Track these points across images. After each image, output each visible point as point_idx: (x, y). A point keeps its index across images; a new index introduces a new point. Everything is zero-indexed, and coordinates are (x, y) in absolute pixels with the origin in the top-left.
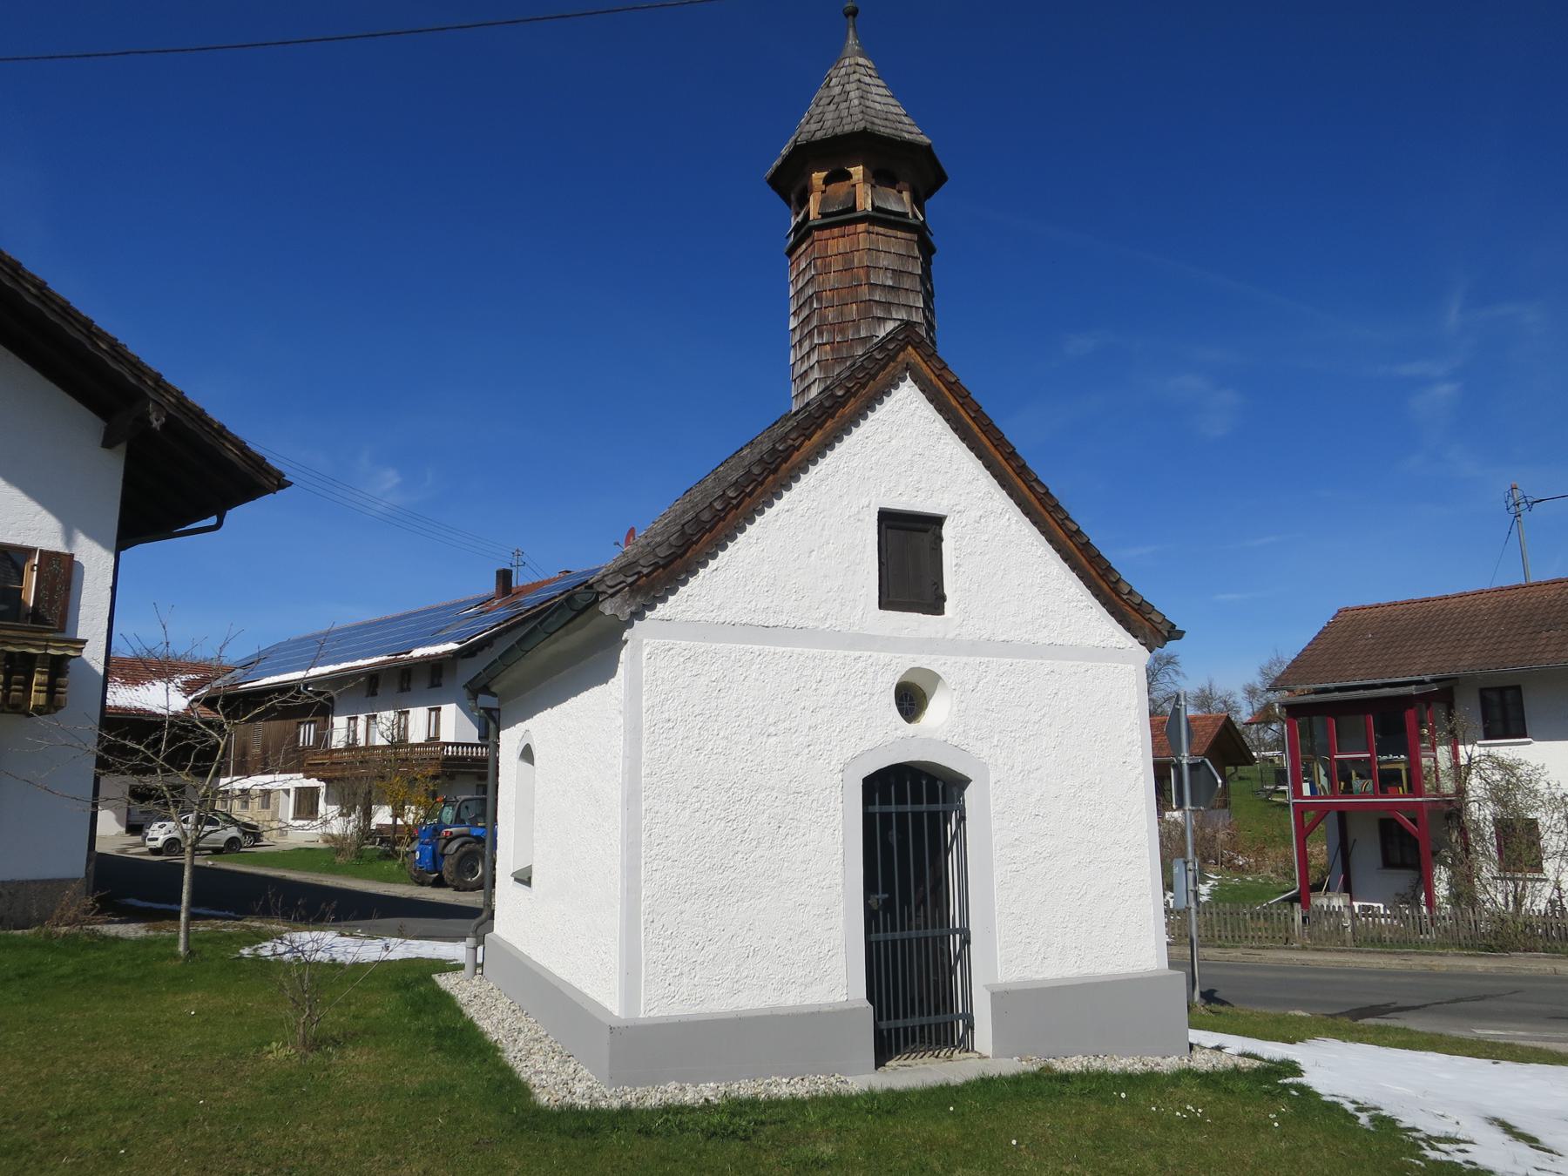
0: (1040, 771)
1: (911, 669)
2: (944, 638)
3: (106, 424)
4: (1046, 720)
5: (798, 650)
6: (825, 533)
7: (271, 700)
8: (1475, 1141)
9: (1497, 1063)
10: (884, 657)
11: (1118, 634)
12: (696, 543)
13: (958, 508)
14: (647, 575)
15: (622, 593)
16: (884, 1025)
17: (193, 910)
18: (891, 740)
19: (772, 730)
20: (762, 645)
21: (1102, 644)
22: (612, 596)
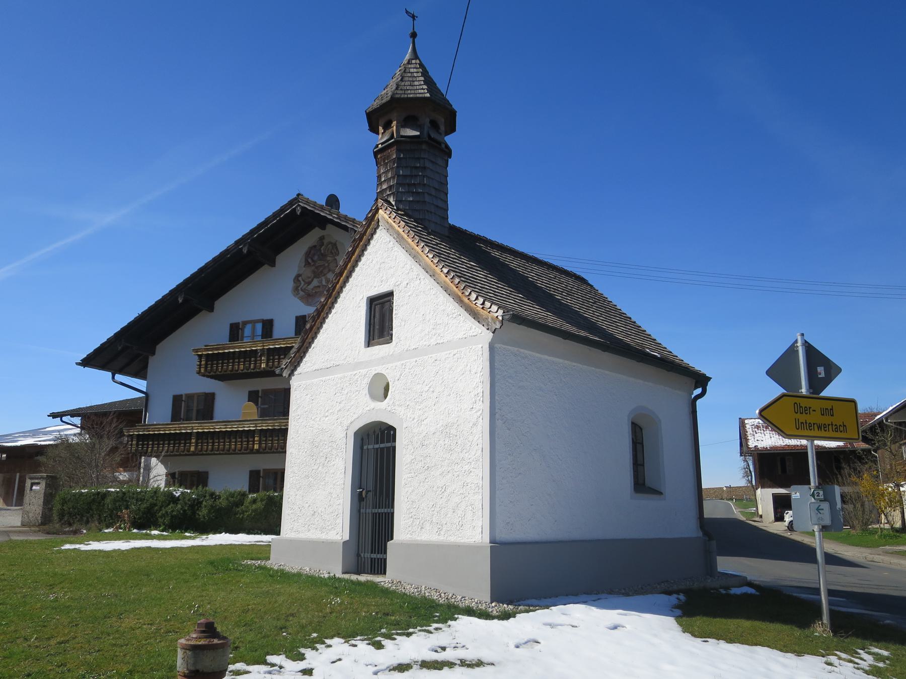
0: (427, 420)
1: (375, 374)
2: (388, 355)
3: (150, 357)
4: (431, 389)
5: (336, 376)
6: (348, 318)
7: (134, 432)
8: (485, 660)
9: (707, 641)
10: (363, 371)
11: (474, 327)
12: (307, 338)
13: (397, 284)
14: (294, 356)
15: (289, 367)
16: (269, 549)
17: (830, 598)
18: (365, 412)
19: (327, 414)
20: (333, 375)
21: (464, 336)
22: (286, 368)
